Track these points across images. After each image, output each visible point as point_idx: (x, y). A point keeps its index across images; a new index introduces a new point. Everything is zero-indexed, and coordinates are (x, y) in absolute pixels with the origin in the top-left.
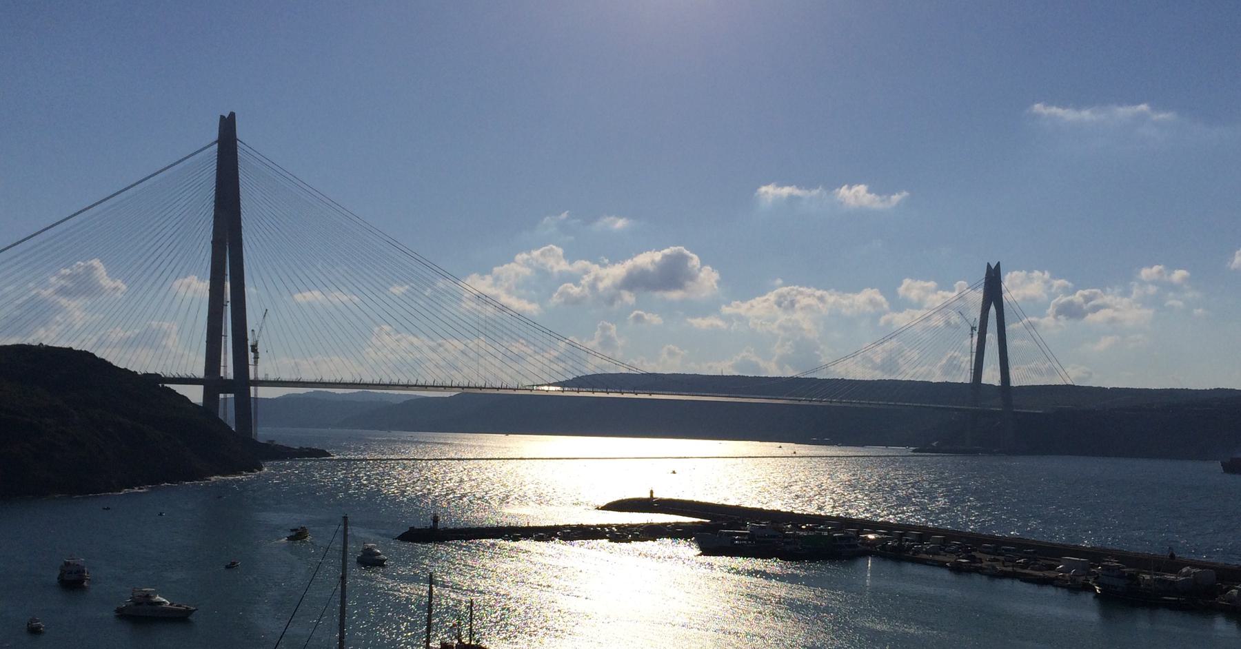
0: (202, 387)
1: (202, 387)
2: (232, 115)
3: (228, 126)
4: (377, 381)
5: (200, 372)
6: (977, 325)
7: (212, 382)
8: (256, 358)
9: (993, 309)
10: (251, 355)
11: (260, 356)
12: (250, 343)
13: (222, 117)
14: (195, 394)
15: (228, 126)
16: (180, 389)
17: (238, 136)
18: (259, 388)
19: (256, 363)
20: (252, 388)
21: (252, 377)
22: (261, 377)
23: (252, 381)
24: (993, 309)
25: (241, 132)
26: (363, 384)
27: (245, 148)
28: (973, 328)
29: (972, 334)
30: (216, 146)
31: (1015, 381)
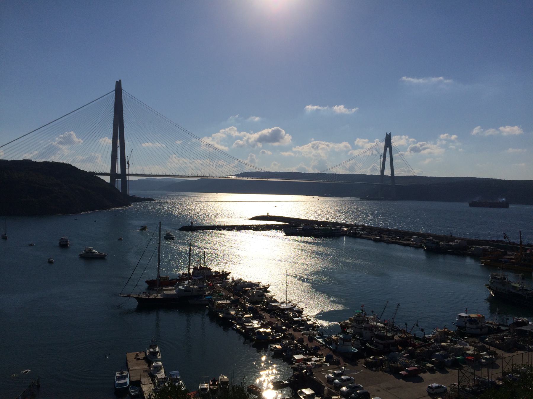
2: (120, 81)
3: (119, 84)
4: (171, 174)
5: (109, 171)
8: (129, 166)
9: (388, 149)
10: (127, 165)
11: (130, 165)
13: (117, 82)
14: (107, 179)
15: (119, 84)
16: (102, 177)
19: (128, 168)
20: (127, 177)
21: (127, 173)
22: (130, 173)
23: (127, 174)
24: (388, 149)
25: (123, 87)
26: (173, 176)
27: (125, 92)
28: (381, 156)
29: (381, 158)
30: (115, 91)
31: (396, 174)
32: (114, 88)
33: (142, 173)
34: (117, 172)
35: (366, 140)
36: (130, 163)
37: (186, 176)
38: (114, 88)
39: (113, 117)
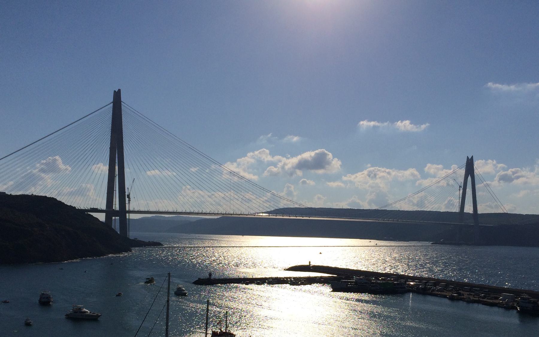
0: (105, 214)
1: (105, 214)
2: (119, 90)
3: (117, 95)
4: (184, 211)
6: (462, 185)
7: (109, 211)
8: (129, 201)
9: (469, 178)
10: (127, 199)
12: (126, 194)
13: (115, 91)
14: (102, 217)
15: (117, 95)
17: (122, 100)
18: (130, 214)
19: (129, 203)
20: (127, 214)
21: (127, 209)
22: (131, 209)
24: (469, 178)
26: (178, 213)
27: (126, 106)
28: (460, 187)
29: (460, 189)
32: (110, 99)
33: (146, 210)
34: (114, 208)
35: (440, 166)
36: (131, 196)
39: (109, 137)
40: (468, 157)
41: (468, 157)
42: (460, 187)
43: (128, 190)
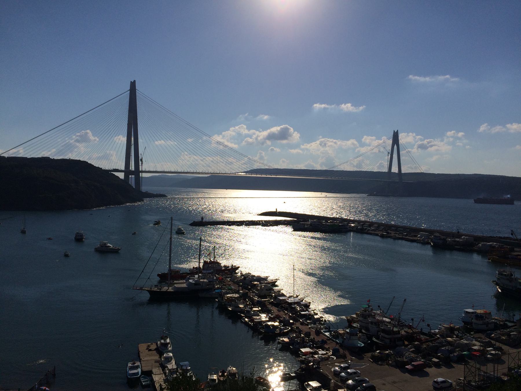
2: (135, 81)
3: (133, 85)
4: (183, 171)
6: (390, 152)
8: (142, 163)
9: (395, 147)
10: (140, 162)
12: (140, 158)
15: (133, 85)
20: (140, 174)
21: (140, 170)
22: (143, 170)
24: (395, 147)
26: (178, 172)
28: (389, 153)
29: (388, 155)
30: (129, 92)
31: (403, 171)
33: (154, 170)
36: (143, 160)
37: (197, 173)
38: (129, 88)
40: (398, 130)
41: (398, 130)
42: (388, 153)
43: (141, 155)
